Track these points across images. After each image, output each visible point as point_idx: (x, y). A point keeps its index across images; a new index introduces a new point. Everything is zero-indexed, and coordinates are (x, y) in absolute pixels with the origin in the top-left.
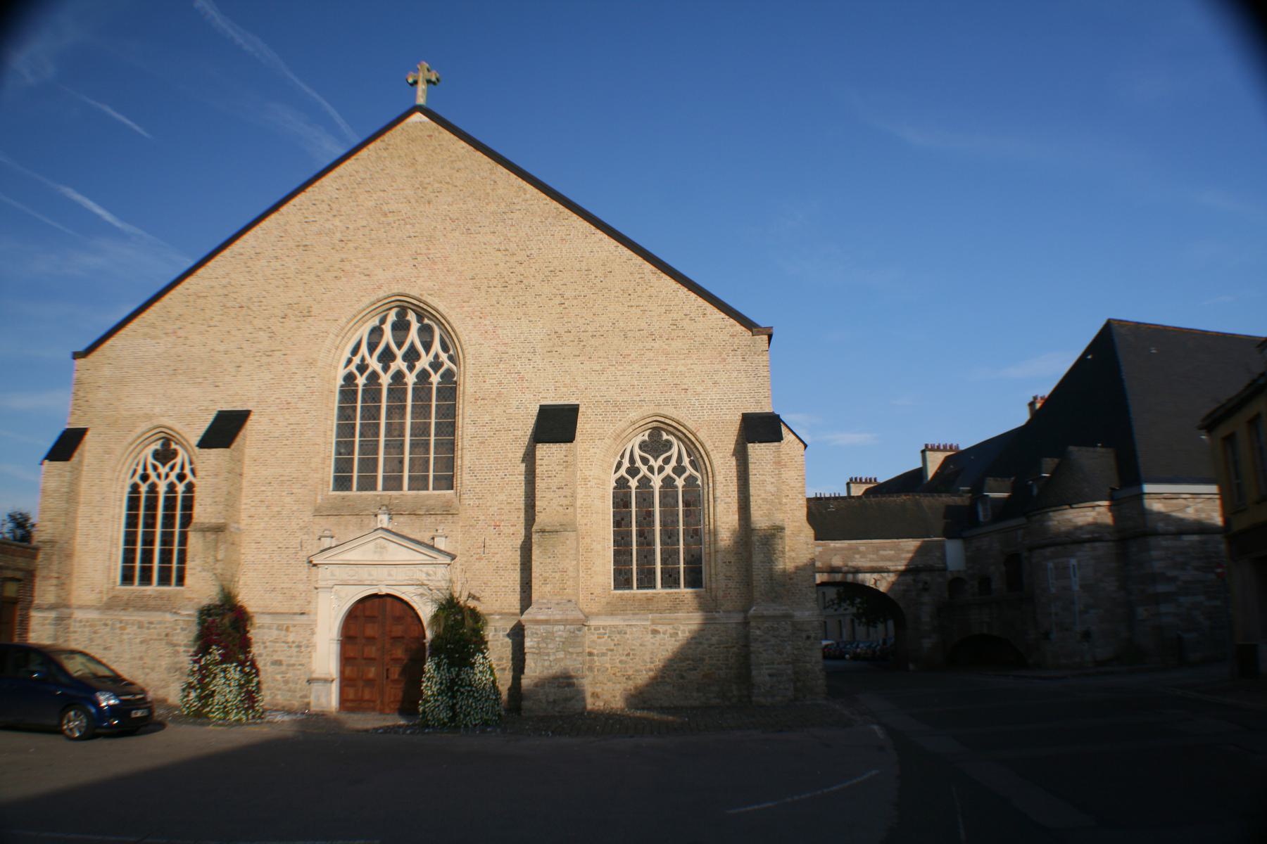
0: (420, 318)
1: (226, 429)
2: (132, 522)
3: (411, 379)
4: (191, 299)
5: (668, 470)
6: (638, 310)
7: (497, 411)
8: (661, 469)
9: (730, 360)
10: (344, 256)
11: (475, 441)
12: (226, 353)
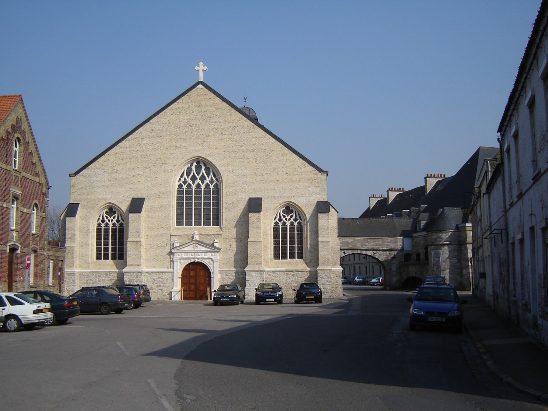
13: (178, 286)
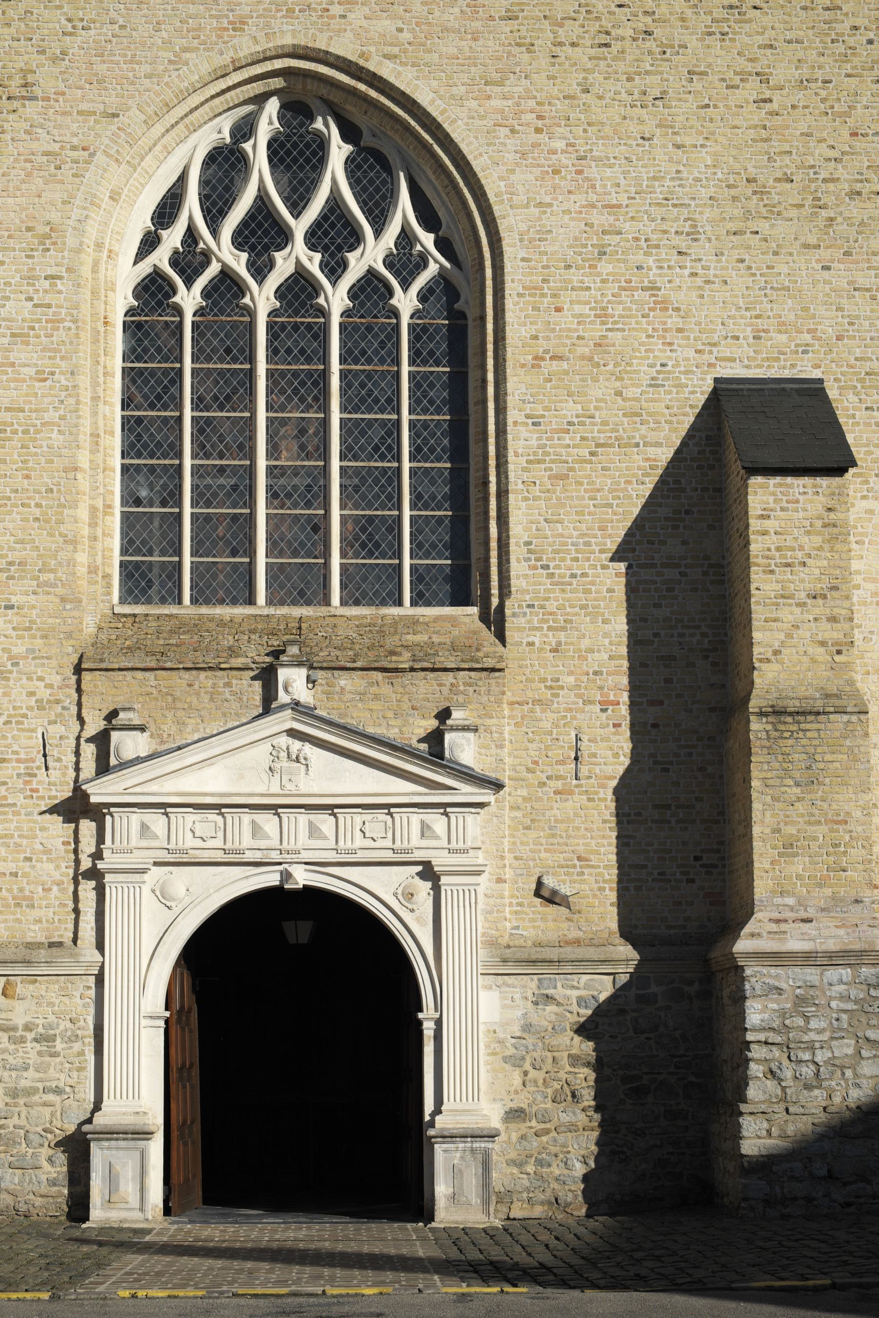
0: (349, 133)
7: (596, 392)
11: (540, 472)
13: (138, 1084)
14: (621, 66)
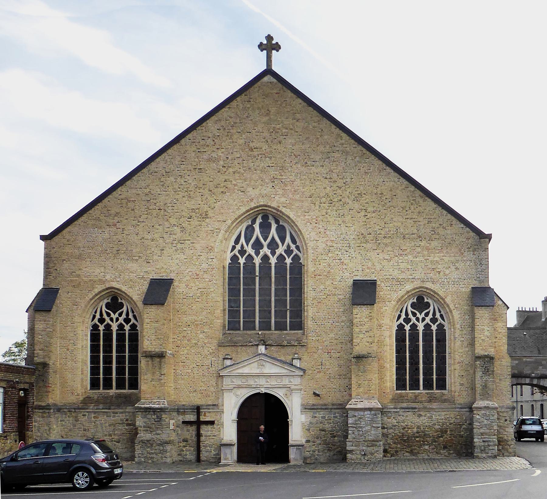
0: (277, 222)
1: (159, 291)
2: (94, 349)
3: (273, 260)
4: (124, 201)
5: (428, 320)
6: (411, 221)
7: (328, 283)
8: (423, 319)
9: (465, 254)
10: (227, 177)
11: (315, 302)
12: (153, 240)
14: (335, 208)
